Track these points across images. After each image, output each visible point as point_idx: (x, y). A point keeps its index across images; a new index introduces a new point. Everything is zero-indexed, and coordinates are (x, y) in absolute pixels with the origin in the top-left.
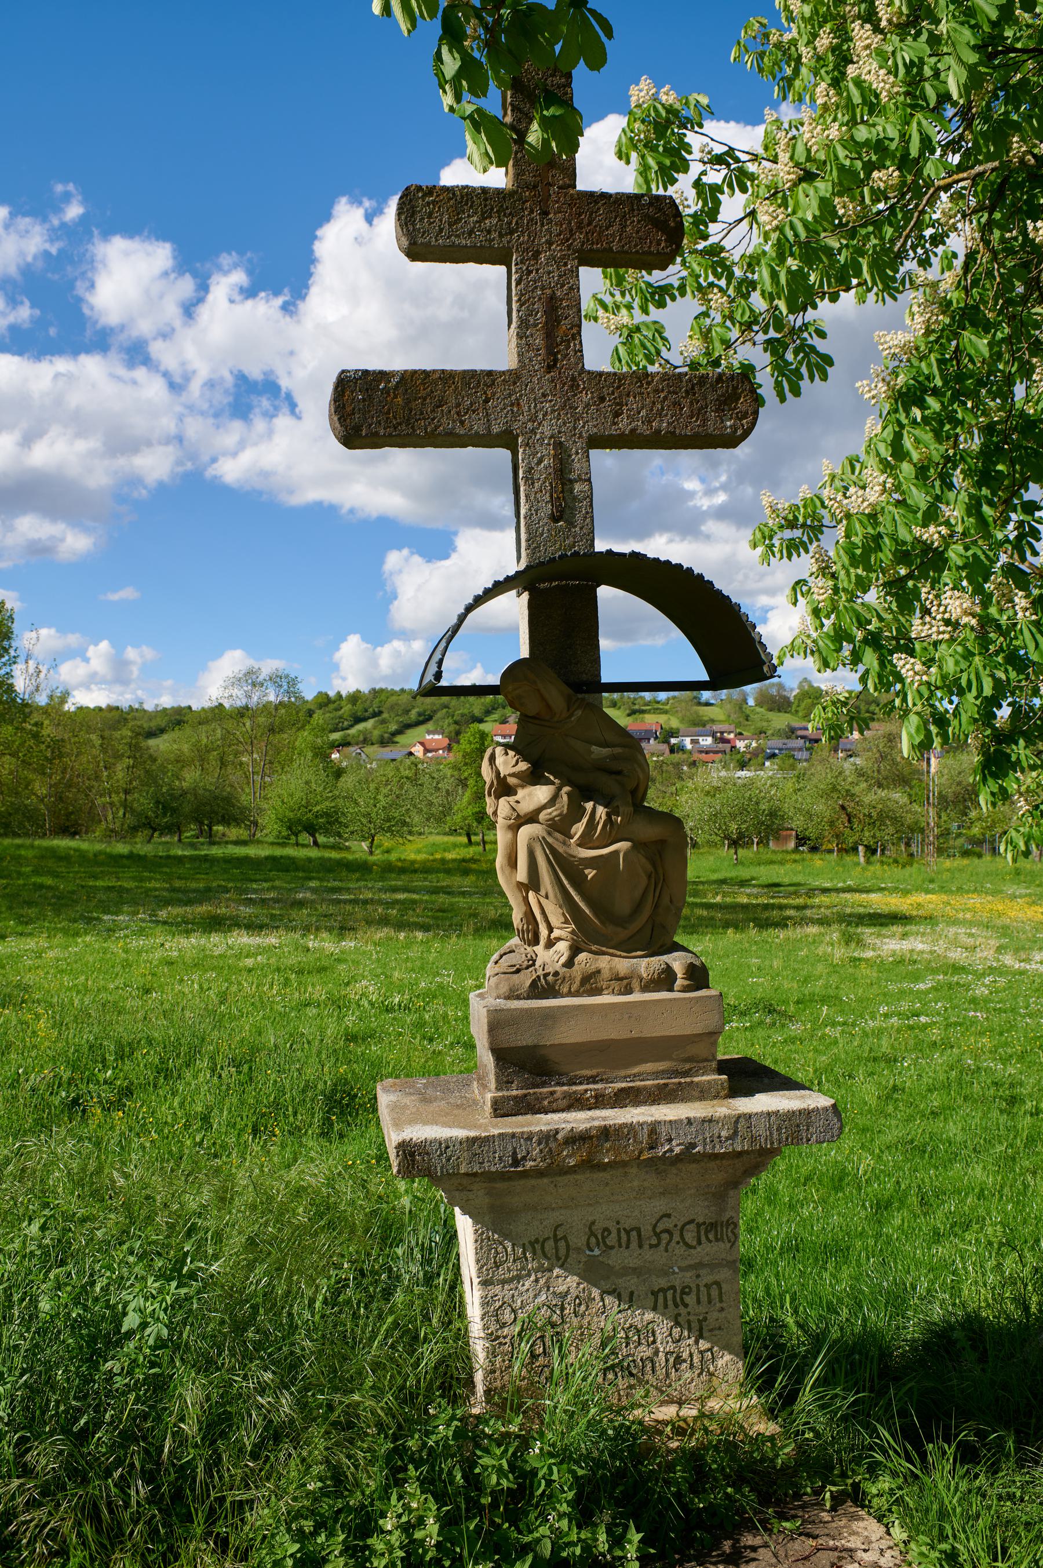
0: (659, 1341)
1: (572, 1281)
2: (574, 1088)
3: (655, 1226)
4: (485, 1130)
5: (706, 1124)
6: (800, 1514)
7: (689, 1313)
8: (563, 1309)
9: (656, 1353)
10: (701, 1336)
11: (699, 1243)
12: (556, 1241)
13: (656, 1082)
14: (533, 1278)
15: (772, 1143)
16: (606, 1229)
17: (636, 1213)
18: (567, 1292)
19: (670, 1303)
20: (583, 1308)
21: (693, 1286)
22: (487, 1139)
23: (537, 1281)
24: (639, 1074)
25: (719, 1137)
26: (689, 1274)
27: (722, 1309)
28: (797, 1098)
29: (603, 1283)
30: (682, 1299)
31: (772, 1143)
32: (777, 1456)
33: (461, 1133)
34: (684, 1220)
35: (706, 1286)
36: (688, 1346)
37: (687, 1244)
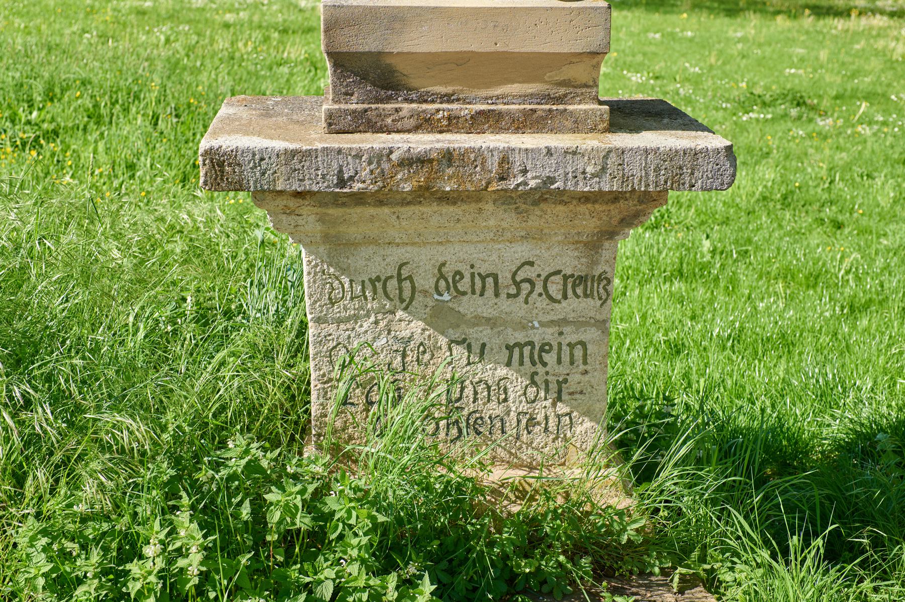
0: (511, 399)
1: (417, 326)
2: (424, 106)
3: (514, 274)
4: (310, 144)
5: (569, 157)
6: (643, 592)
7: (547, 373)
8: (404, 356)
9: (508, 413)
10: (559, 399)
11: (565, 297)
12: (400, 280)
13: (522, 107)
14: (372, 319)
15: (647, 185)
16: (458, 273)
17: (494, 257)
18: (410, 338)
19: (527, 360)
20: (427, 356)
21: (555, 345)
22: (309, 153)
23: (376, 322)
24: (503, 96)
25: (584, 173)
26: (550, 330)
27: (586, 372)
28: (689, 137)
29: (451, 331)
30: (540, 357)
31: (647, 185)
32: (624, 530)
33: (279, 145)
34: (549, 270)
35: (569, 345)
36: (543, 408)
37: (550, 298)
